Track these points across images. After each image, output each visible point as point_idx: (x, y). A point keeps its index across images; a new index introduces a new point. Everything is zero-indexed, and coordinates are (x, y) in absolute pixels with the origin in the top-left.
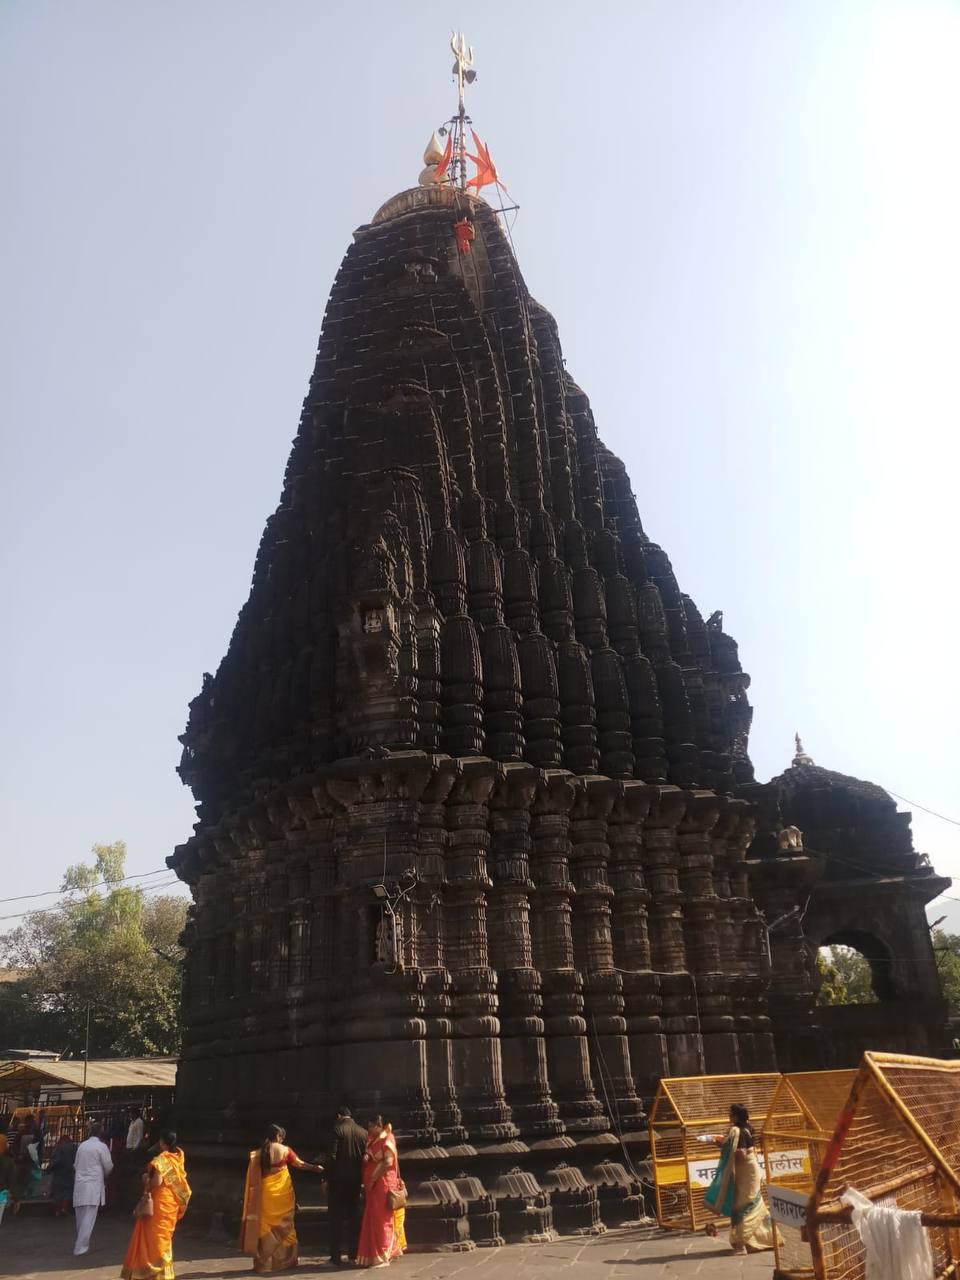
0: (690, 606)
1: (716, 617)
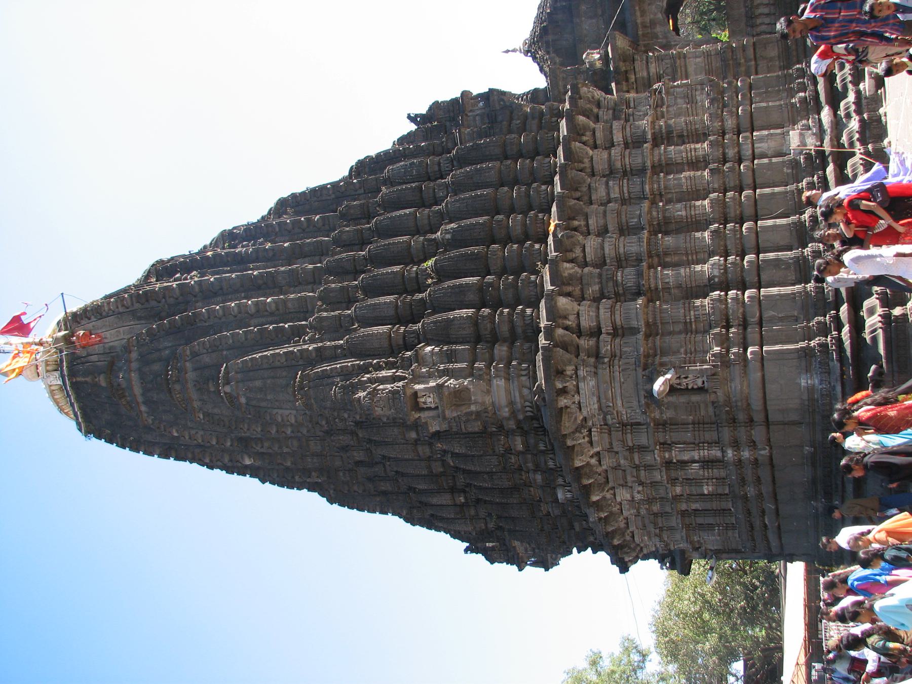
0: (402, 140)
1: (412, 119)
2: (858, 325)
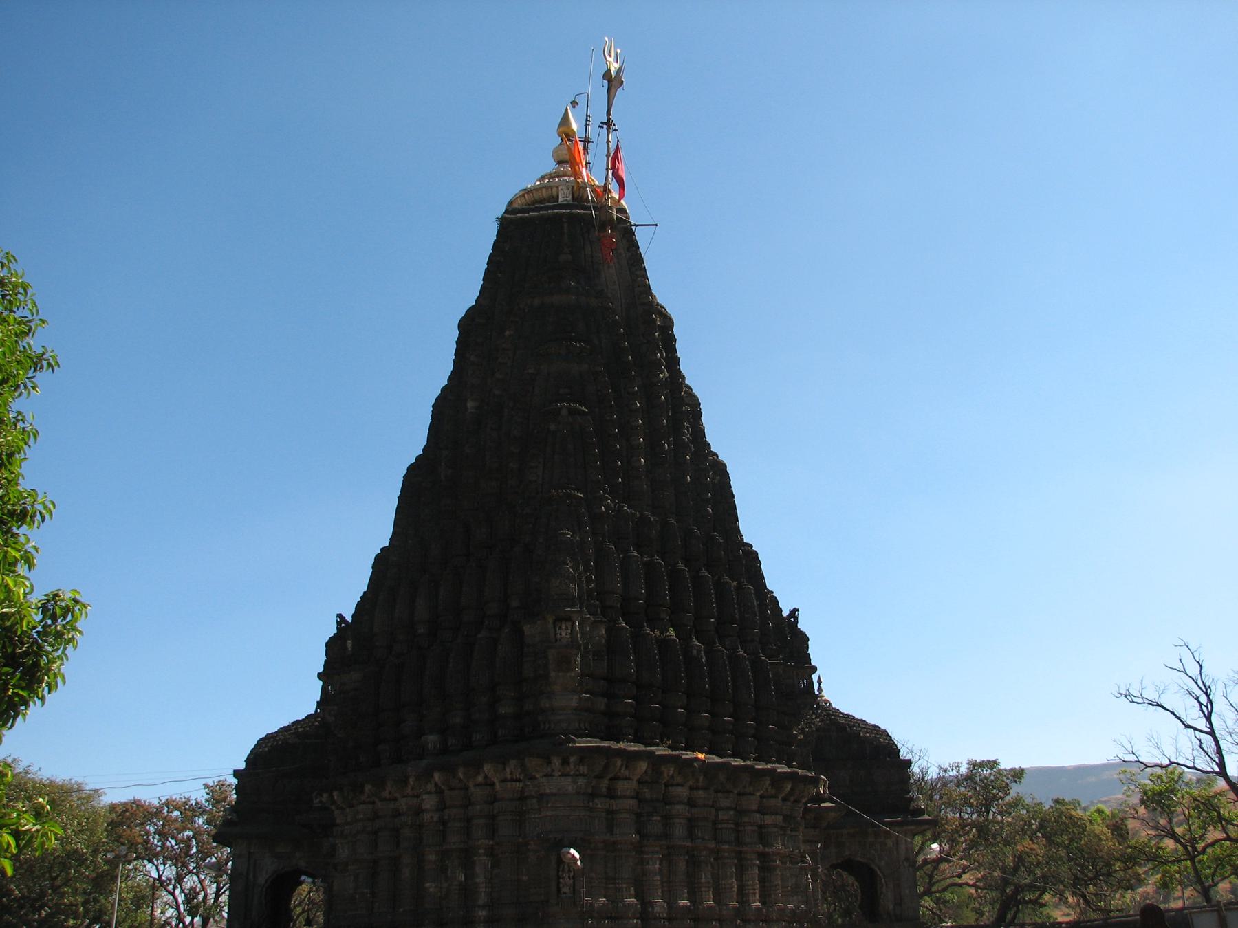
0: (775, 601)
1: (794, 613)
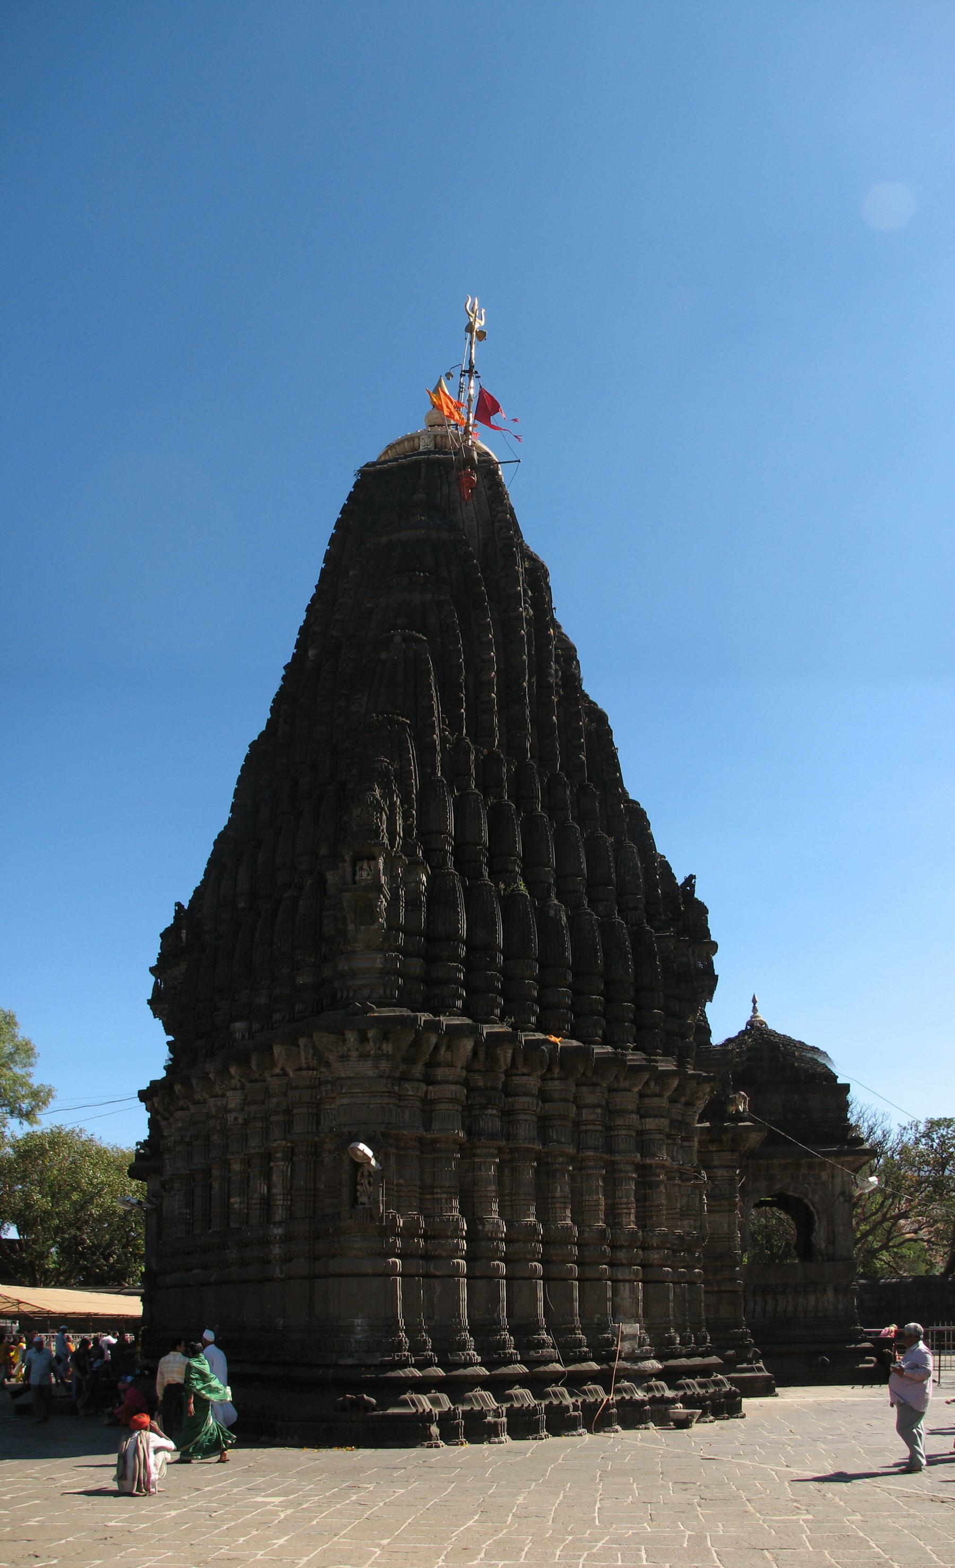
0: (666, 866)
1: (690, 880)
2: (422, 1386)
